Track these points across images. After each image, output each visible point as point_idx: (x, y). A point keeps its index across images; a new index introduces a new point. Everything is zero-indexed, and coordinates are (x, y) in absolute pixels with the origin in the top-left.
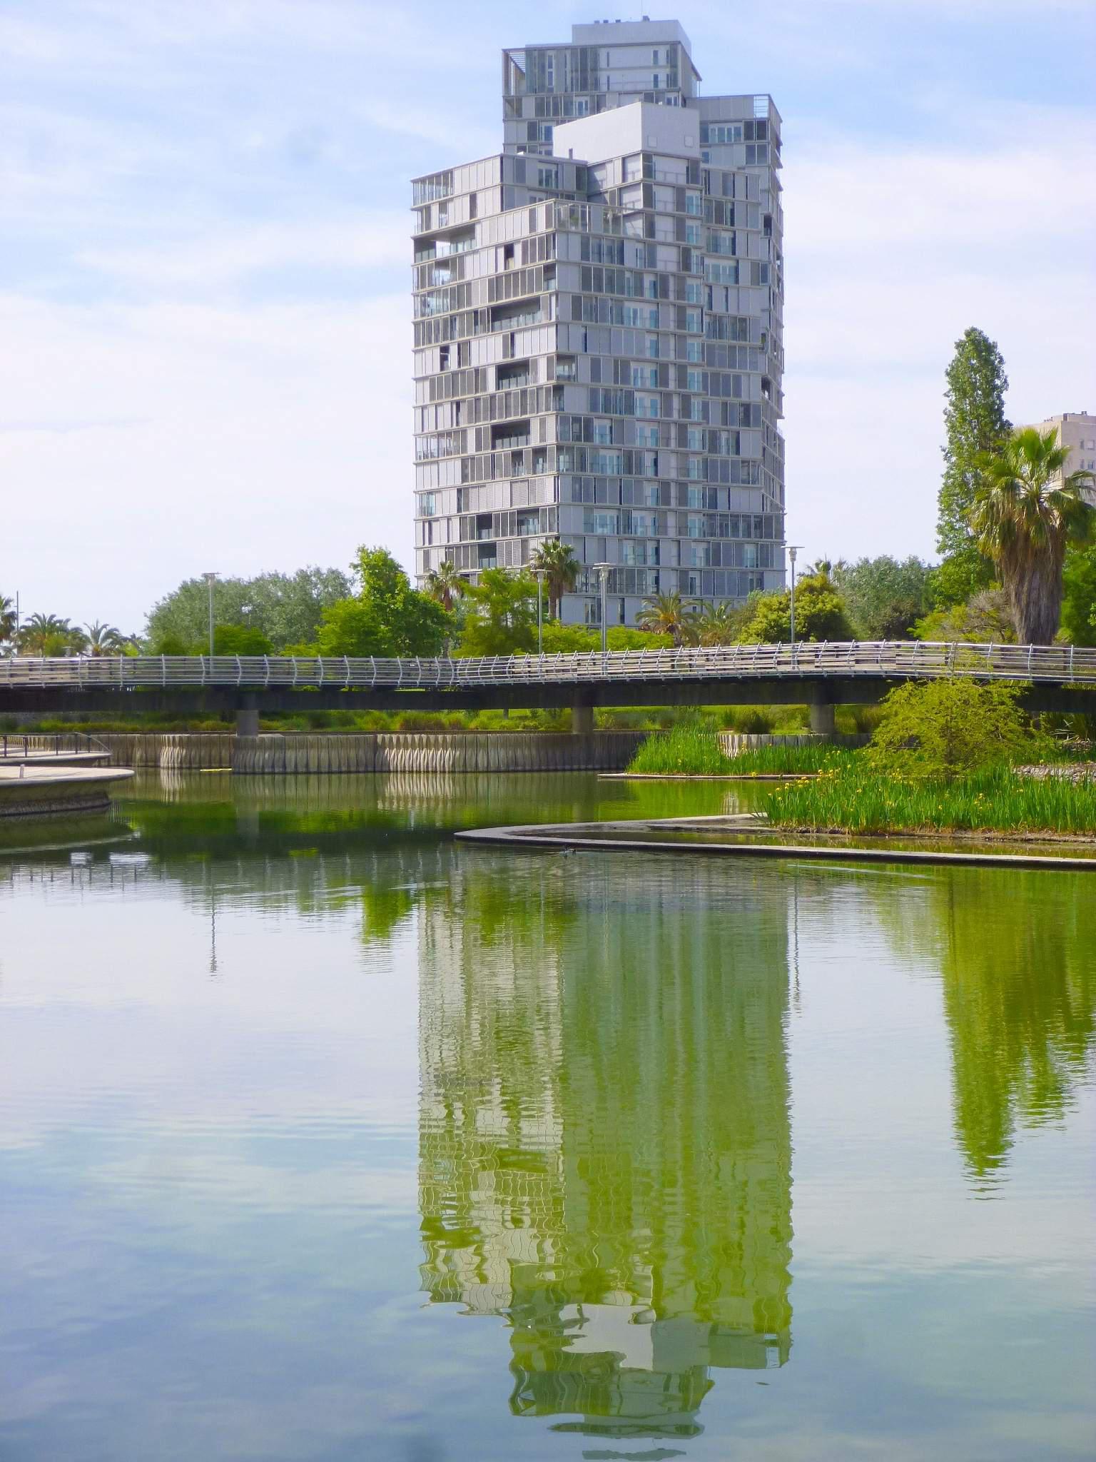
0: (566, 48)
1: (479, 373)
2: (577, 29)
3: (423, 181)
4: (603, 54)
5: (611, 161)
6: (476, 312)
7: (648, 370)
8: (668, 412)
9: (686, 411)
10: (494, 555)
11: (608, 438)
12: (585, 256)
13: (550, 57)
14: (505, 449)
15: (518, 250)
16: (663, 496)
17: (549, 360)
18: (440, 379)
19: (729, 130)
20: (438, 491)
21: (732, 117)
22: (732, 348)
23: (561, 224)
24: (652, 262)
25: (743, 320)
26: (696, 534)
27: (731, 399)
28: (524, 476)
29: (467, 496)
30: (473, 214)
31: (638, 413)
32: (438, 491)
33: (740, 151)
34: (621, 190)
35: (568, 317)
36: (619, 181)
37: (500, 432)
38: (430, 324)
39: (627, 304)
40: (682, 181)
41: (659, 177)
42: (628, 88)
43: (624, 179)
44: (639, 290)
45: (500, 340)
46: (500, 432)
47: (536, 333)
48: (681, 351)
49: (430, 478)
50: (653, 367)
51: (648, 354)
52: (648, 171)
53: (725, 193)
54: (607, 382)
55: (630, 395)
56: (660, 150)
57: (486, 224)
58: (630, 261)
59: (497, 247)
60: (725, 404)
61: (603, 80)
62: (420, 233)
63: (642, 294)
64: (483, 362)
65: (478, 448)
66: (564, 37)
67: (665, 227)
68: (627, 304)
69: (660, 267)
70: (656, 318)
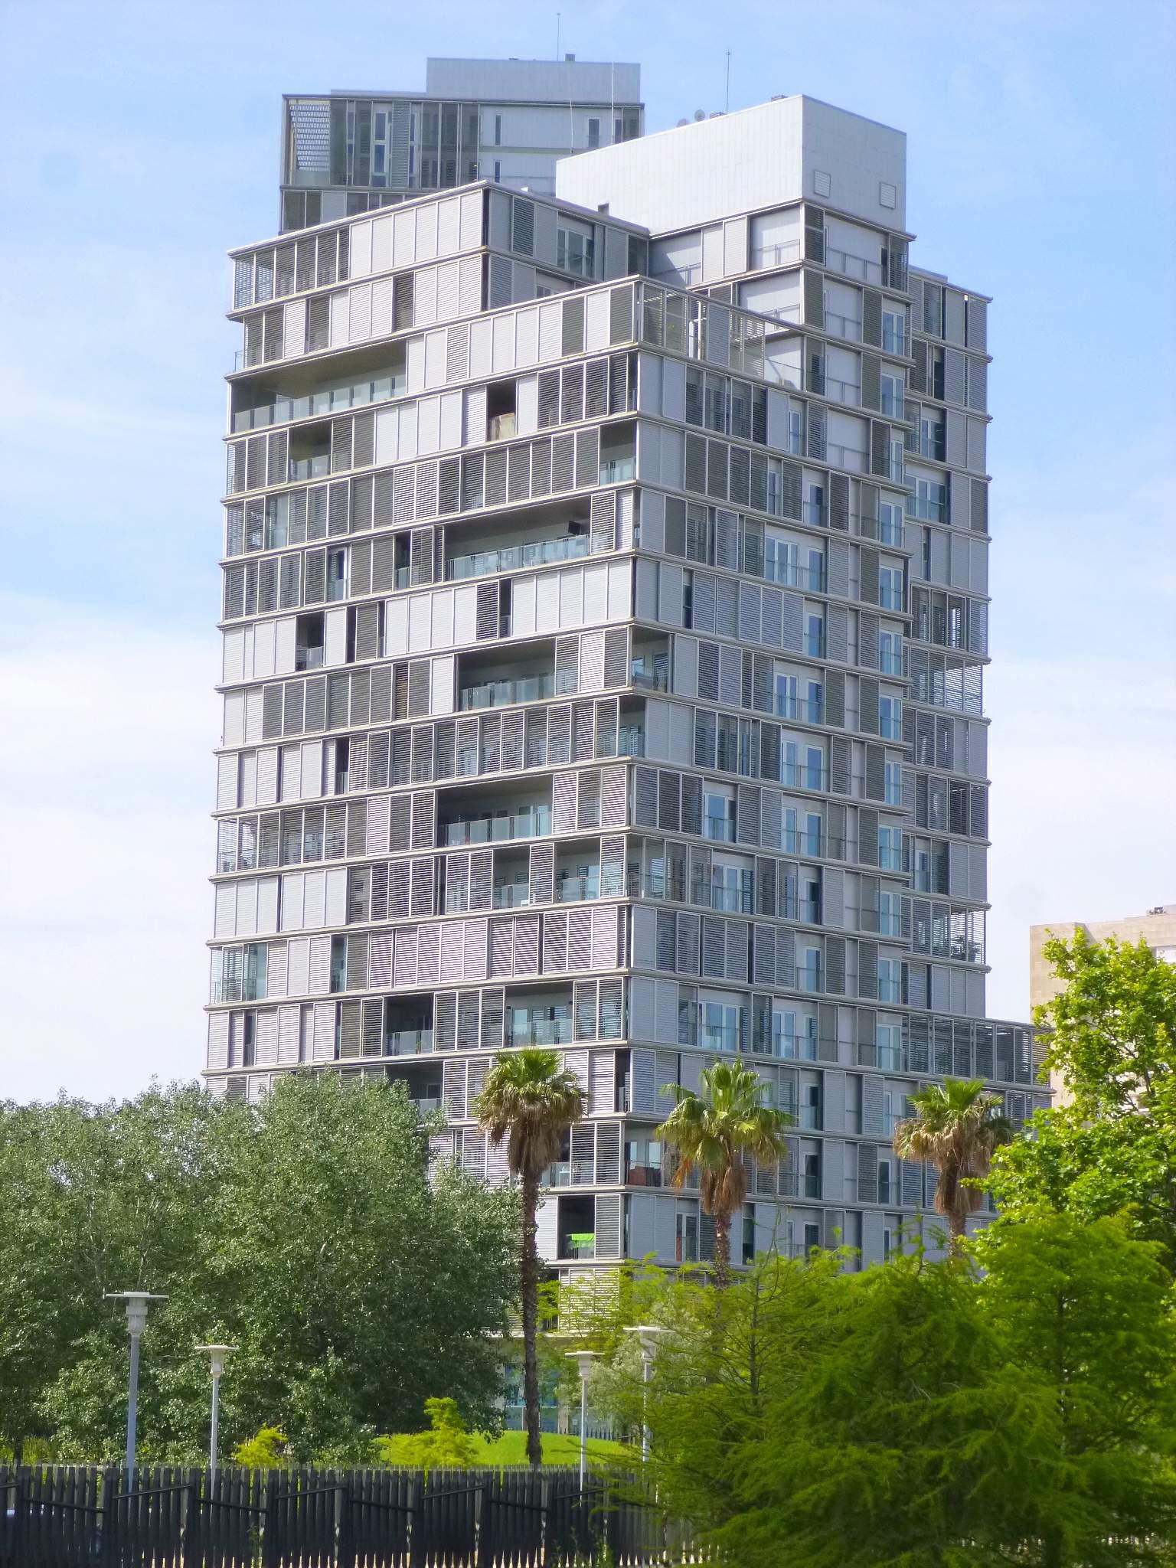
0: (416, 101)
1: (407, 676)
2: (436, 67)
4: (487, 119)
5: (716, 225)
6: (402, 539)
7: (806, 680)
8: (840, 781)
9: (875, 784)
10: (435, 1093)
11: (727, 826)
12: (693, 415)
13: (381, 118)
14: (470, 845)
15: (528, 396)
16: (828, 972)
17: (613, 638)
18: (294, 689)
20: (280, 942)
24: (818, 447)
26: (888, 1064)
27: (935, 772)
28: (526, 905)
29: (359, 953)
32: (280, 942)
35: (660, 548)
36: (738, 266)
37: (459, 807)
38: (270, 567)
40: (874, 277)
43: (751, 265)
44: (793, 506)
45: (468, 599)
46: (459, 807)
47: (573, 580)
48: (867, 651)
49: (253, 912)
51: (805, 651)
52: (815, 246)
53: (928, 328)
54: (729, 704)
55: (771, 734)
57: (438, 343)
58: (781, 436)
59: (467, 390)
62: (243, 368)
63: (797, 515)
64: (420, 647)
65: (398, 842)
66: (409, 79)
67: (840, 368)
68: (770, 532)
69: (832, 459)
70: (821, 565)
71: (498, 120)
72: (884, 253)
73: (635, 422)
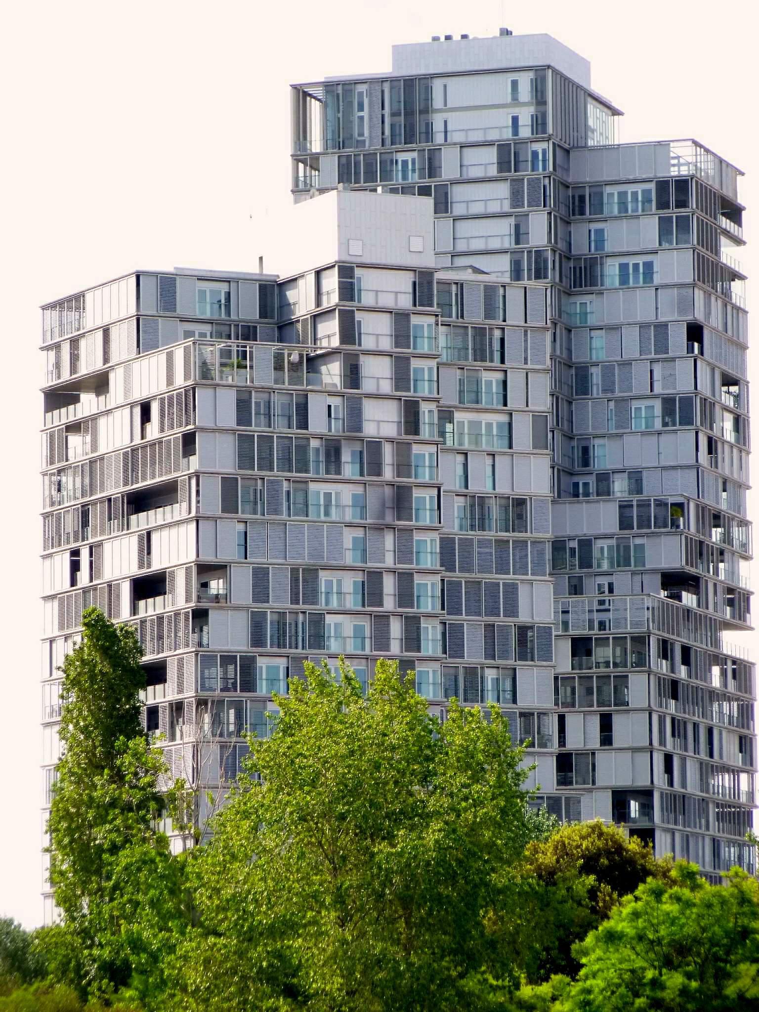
0: (383, 81)
3: (52, 306)
4: (437, 85)
5: (302, 276)
7: (349, 582)
9: (412, 640)
13: (361, 94)
14: (606, 606)
17: (188, 570)
19: (635, 194)
21: (638, 175)
22: (502, 544)
23: (205, 372)
25: (520, 503)
27: (501, 620)
30: (106, 360)
31: (334, 646)
33: (649, 227)
34: (315, 318)
39: (313, 487)
40: (405, 302)
41: (367, 299)
42: (475, 137)
43: (318, 303)
45: (134, 540)
47: (174, 531)
50: (359, 577)
52: (348, 290)
54: (279, 600)
55: (317, 621)
56: (367, 260)
59: (132, 406)
60: (490, 627)
61: (438, 126)
64: (117, 575)
66: (379, 63)
67: (377, 373)
68: (313, 487)
69: (369, 430)
71: (445, 86)
72: (414, 283)
73: (195, 432)
